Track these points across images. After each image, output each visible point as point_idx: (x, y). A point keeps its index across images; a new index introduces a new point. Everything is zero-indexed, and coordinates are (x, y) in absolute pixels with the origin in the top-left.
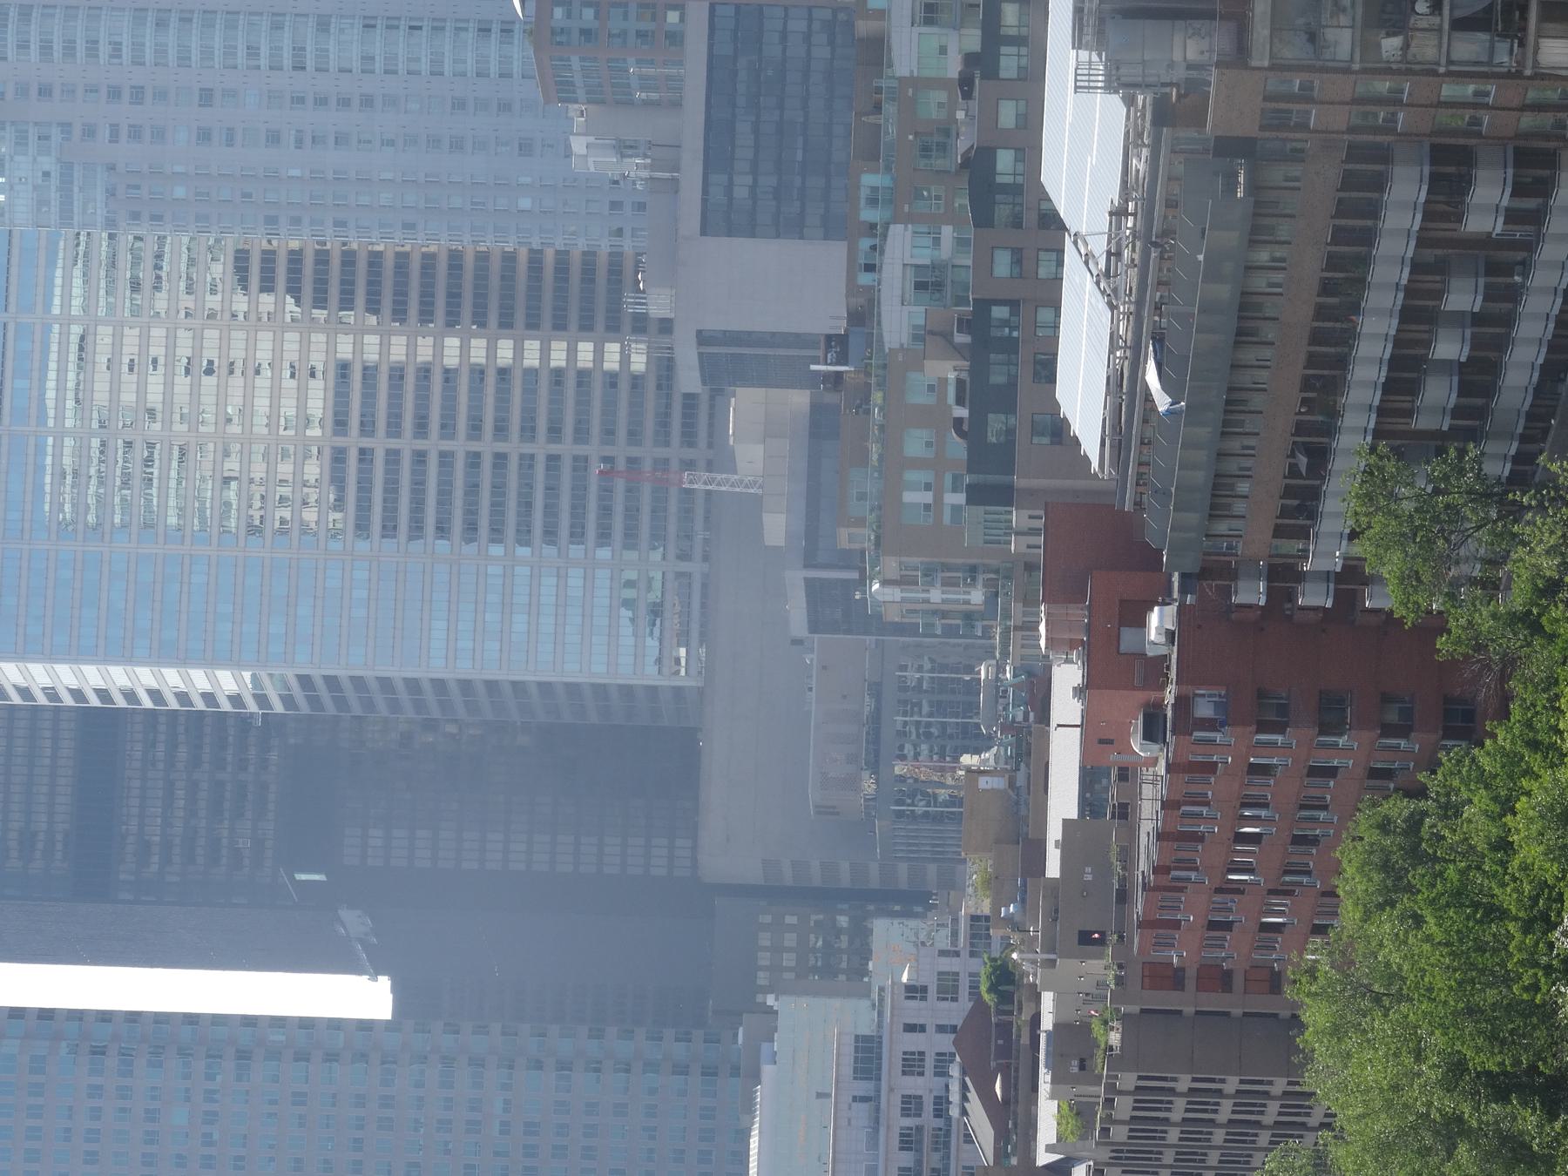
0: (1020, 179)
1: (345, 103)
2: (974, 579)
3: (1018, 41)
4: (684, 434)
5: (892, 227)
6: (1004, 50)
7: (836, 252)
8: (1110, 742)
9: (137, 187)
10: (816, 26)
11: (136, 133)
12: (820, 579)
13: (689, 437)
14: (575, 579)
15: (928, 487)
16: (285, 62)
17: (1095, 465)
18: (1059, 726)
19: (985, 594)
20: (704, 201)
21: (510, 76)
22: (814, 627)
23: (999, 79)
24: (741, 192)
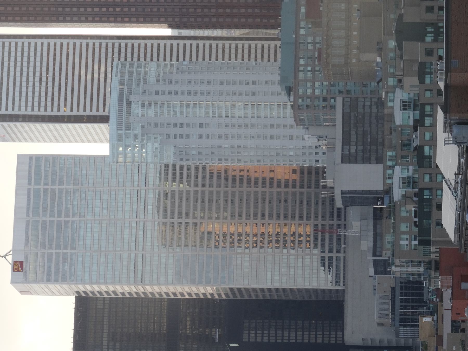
0: (431, 154)
1: (240, 126)
2: (420, 265)
3: (430, 116)
4: (337, 217)
5: (395, 167)
6: (427, 76)
7: (380, 167)
8: (459, 314)
9: (182, 151)
10: (373, 103)
11: (181, 136)
12: (377, 260)
13: (339, 218)
14: (308, 259)
15: (407, 239)
16: (223, 115)
17: (453, 241)
18: (445, 309)
19: (424, 269)
20: (342, 154)
21: (286, 117)
22: (376, 273)
23: (424, 126)
24: (353, 151)
